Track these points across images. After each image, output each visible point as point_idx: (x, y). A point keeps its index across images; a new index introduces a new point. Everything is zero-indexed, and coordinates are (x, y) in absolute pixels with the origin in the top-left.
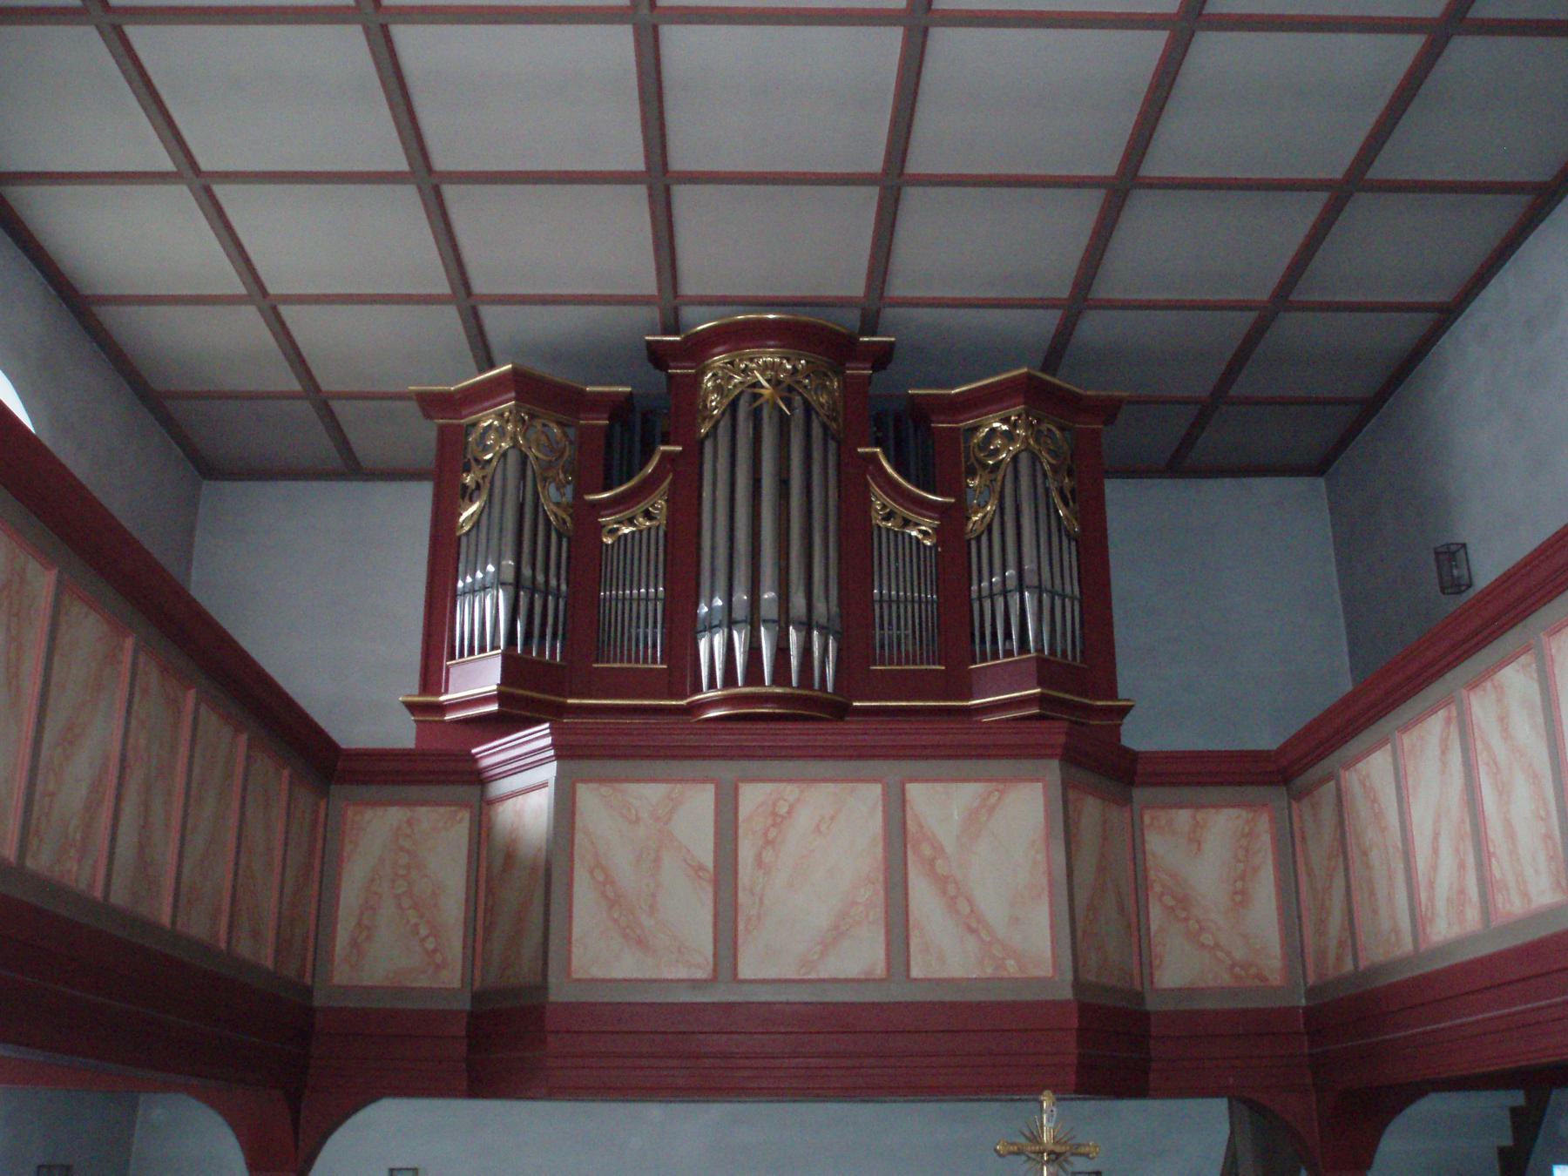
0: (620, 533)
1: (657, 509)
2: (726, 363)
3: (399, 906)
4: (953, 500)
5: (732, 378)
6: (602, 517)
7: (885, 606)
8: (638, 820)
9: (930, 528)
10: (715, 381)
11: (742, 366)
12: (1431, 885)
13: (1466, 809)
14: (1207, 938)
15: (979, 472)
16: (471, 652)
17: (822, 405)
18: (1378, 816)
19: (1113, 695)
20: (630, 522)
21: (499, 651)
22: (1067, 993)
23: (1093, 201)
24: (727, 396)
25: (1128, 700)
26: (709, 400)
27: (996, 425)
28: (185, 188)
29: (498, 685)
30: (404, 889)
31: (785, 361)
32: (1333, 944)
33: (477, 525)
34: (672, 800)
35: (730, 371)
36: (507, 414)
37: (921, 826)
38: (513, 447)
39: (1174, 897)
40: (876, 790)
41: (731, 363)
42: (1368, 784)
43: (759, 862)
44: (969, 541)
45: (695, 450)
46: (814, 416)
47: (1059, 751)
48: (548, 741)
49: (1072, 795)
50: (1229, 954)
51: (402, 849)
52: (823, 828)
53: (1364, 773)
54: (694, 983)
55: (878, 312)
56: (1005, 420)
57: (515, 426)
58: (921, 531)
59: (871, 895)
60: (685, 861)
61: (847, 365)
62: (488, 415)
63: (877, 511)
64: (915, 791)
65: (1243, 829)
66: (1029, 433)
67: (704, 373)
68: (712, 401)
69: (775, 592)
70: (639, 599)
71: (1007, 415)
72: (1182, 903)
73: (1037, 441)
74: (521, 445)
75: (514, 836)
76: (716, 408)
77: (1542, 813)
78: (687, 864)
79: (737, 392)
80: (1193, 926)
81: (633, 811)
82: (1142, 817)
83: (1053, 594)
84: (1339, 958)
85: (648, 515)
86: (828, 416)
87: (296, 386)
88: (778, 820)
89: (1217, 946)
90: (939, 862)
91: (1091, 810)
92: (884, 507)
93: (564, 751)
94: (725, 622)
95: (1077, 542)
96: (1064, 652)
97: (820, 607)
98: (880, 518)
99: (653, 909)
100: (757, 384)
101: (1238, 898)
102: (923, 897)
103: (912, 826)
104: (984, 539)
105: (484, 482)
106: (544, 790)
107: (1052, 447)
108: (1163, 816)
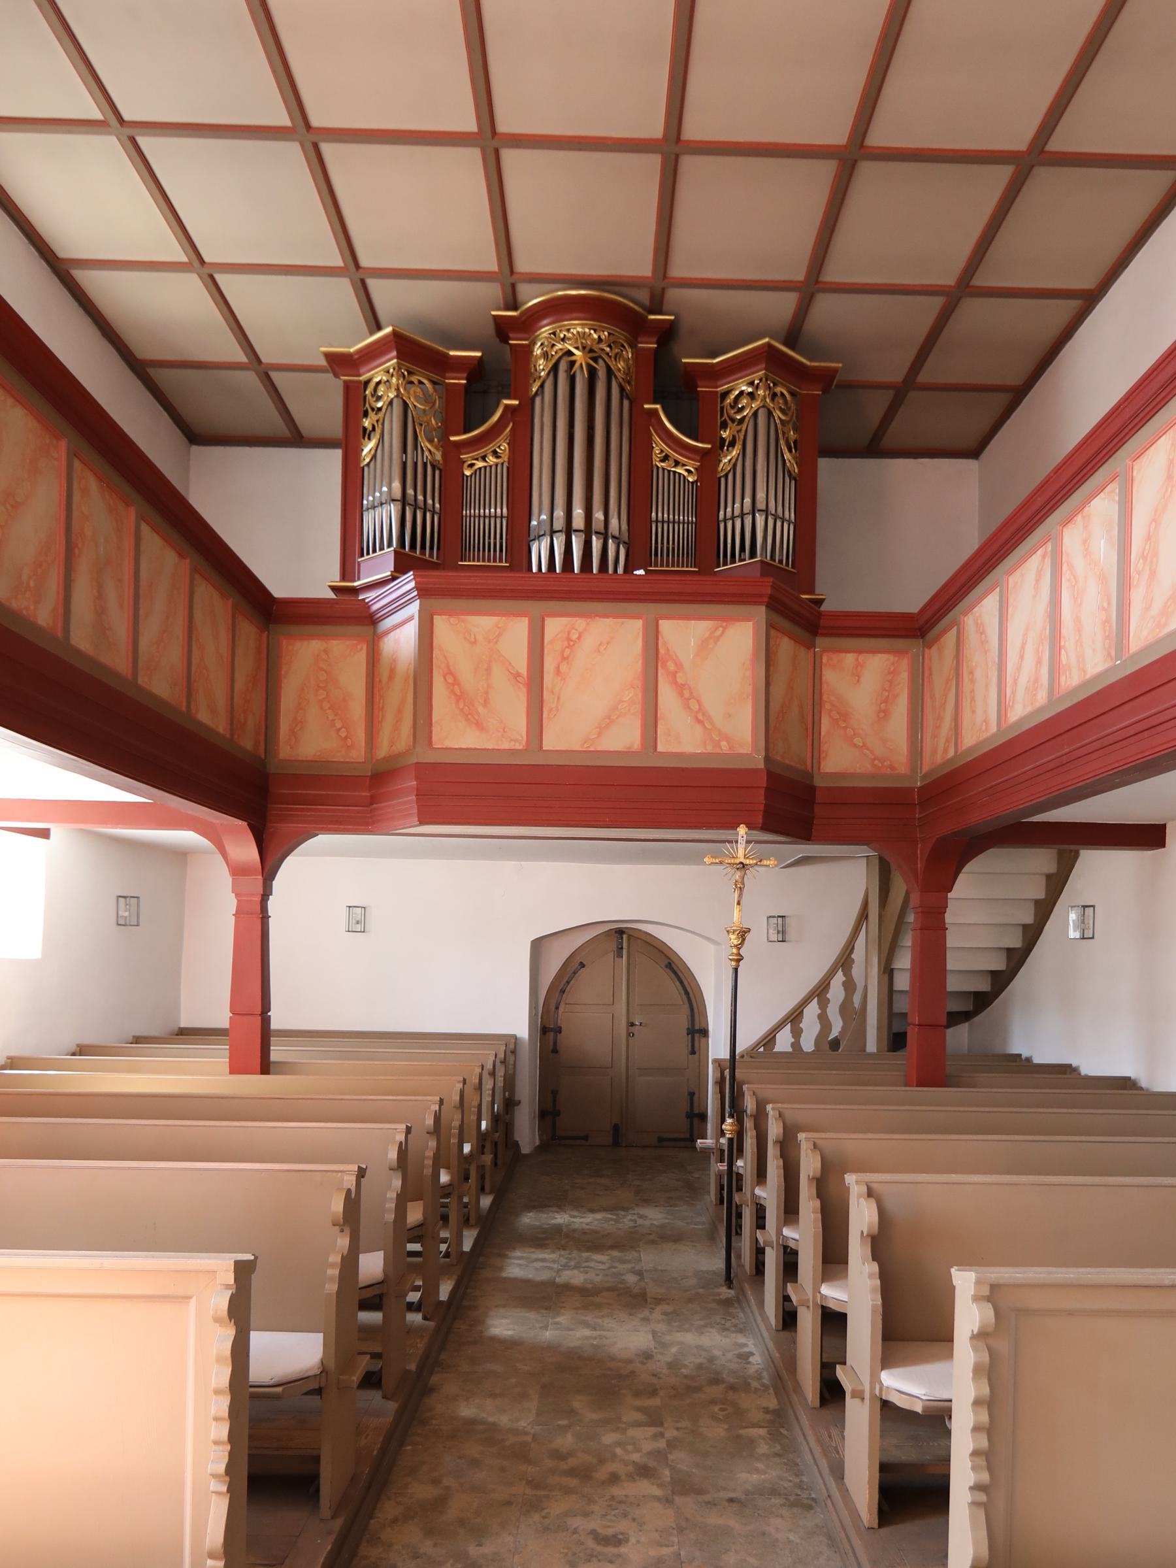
0: (476, 467)
1: (501, 450)
2: (550, 334)
3: (321, 708)
4: (709, 446)
5: (553, 345)
6: (462, 454)
7: (660, 525)
8: (475, 642)
9: (693, 467)
10: (542, 349)
11: (562, 336)
12: (1015, 681)
13: (1048, 620)
14: (858, 741)
15: (729, 426)
16: (374, 551)
17: (619, 370)
18: (984, 642)
19: (812, 592)
20: (484, 458)
21: (392, 549)
22: (761, 765)
23: (826, 170)
24: (551, 359)
25: (822, 595)
26: (538, 364)
27: (744, 388)
28: (114, 139)
29: (392, 572)
30: (324, 696)
31: (592, 332)
32: (943, 740)
33: (374, 457)
34: (499, 628)
35: (553, 340)
36: (391, 370)
37: (668, 650)
38: (397, 396)
39: (838, 713)
40: (638, 624)
41: (554, 333)
42: (979, 622)
43: (558, 671)
44: (720, 479)
45: (528, 404)
46: (613, 379)
47: (766, 604)
48: (412, 584)
49: (773, 632)
50: (872, 752)
51: (322, 669)
52: (602, 649)
53: (977, 614)
54: (513, 752)
55: (663, 290)
56: (751, 384)
57: (398, 379)
58: (687, 470)
59: (633, 696)
60: (508, 670)
61: (639, 339)
62: (377, 373)
63: (656, 454)
64: (666, 626)
65: (890, 668)
66: (767, 393)
67: (534, 343)
68: (539, 366)
69: (582, 510)
70: (490, 517)
71: (752, 380)
72: (843, 716)
73: (773, 399)
74: (402, 394)
75: (394, 657)
76: (543, 370)
77: (1105, 605)
78: (510, 672)
79: (557, 357)
80: (850, 732)
81: (473, 636)
82: (821, 658)
83: (776, 517)
84: (946, 750)
85: (495, 453)
86: (623, 379)
87: (243, 358)
88: (571, 643)
89: (865, 746)
90: (679, 675)
91: (785, 646)
92: (662, 451)
93: (423, 592)
94: (548, 532)
95: (796, 480)
96: (781, 562)
97: (614, 522)
98: (658, 459)
99: (486, 702)
100: (570, 353)
101: (882, 715)
102: (667, 696)
103: (662, 651)
104: (730, 477)
105: (378, 425)
106: (413, 622)
107: (783, 407)
108: (835, 657)
